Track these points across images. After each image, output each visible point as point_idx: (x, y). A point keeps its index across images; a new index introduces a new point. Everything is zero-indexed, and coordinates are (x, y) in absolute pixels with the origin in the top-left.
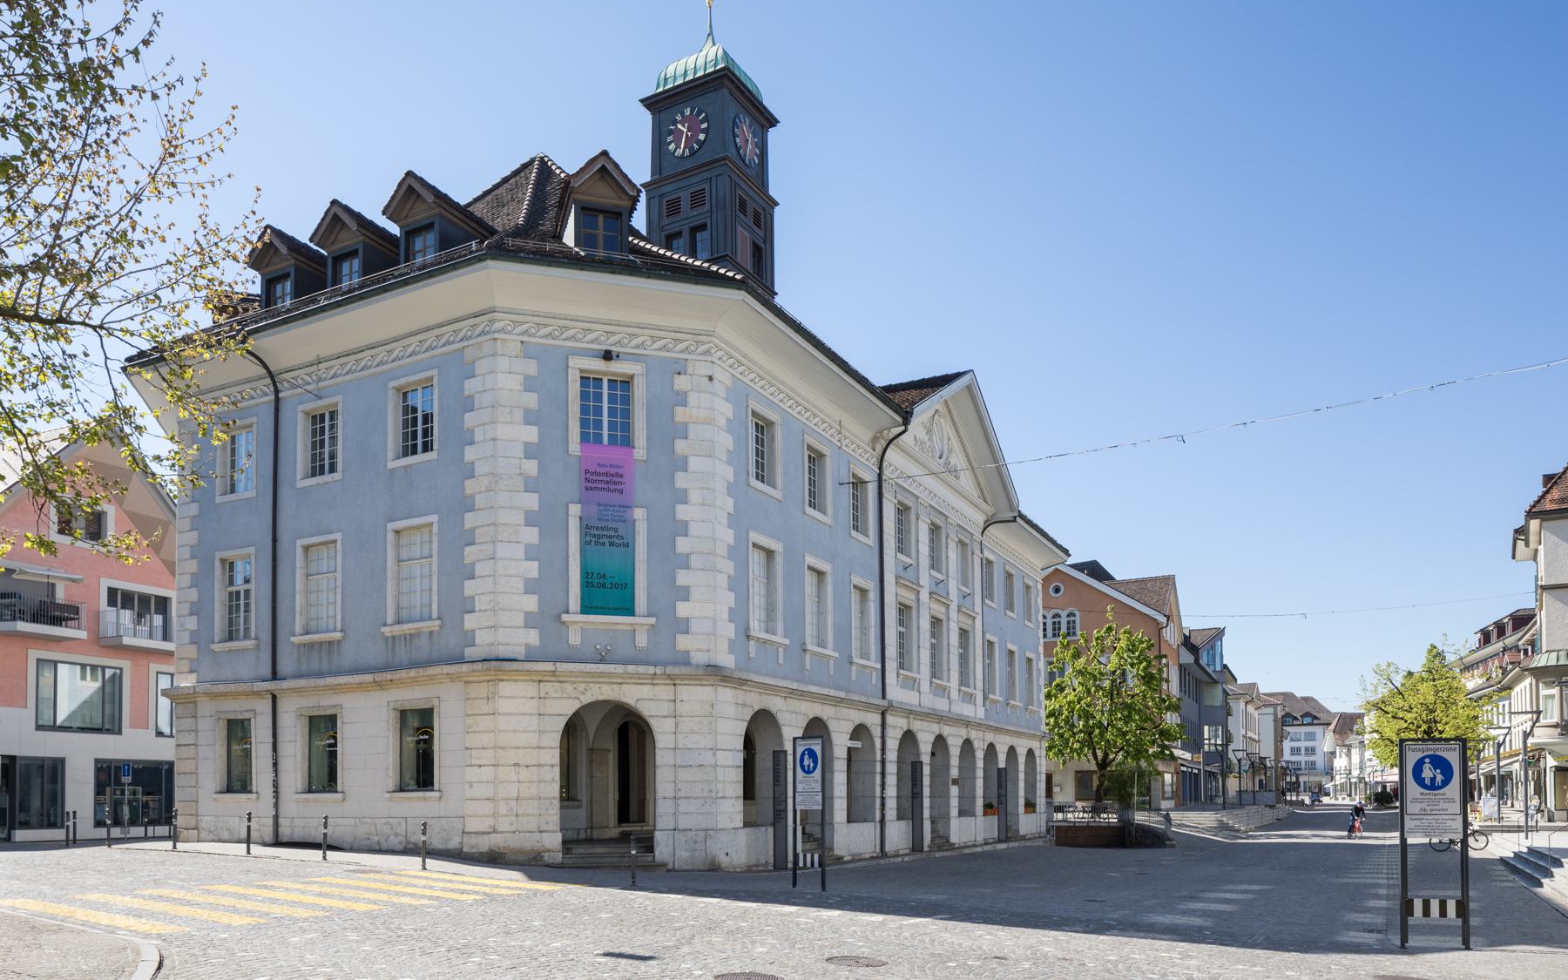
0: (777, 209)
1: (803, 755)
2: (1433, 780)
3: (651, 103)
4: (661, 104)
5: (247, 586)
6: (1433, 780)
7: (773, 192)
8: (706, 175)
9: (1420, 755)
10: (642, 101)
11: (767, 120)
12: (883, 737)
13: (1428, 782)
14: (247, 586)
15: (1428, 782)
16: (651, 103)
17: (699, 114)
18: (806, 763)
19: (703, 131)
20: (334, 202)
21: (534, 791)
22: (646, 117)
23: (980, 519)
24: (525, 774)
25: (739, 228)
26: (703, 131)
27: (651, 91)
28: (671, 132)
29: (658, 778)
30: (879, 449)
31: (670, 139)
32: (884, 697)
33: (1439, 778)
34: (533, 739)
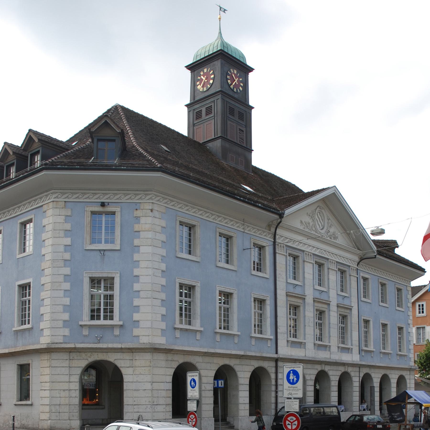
0: (253, 110)
1: (191, 381)
2: (293, 380)
3: (189, 67)
4: (194, 67)
5: (184, 302)
6: (293, 380)
7: (251, 103)
8: (212, 100)
9: (290, 369)
10: (186, 67)
11: (247, 70)
12: (276, 373)
13: (291, 381)
14: (184, 302)
15: (291, 381)
16: (189, 67)
17: (210, 71)
18: (192, 384)
19: (212, 79)
20: (30, 130)
21: (67, 402)
22: (188, 73)
23: (357, 259)
24: (63, 394)
25: (229, 122)
26: (212, 79)
27: (190, 61)
28: (198, 80)
29: (125, 396)
30: (273, 230)
31: (198, 83)
32: (277, 353)
33: (295, 379)
34: (66, 378)
